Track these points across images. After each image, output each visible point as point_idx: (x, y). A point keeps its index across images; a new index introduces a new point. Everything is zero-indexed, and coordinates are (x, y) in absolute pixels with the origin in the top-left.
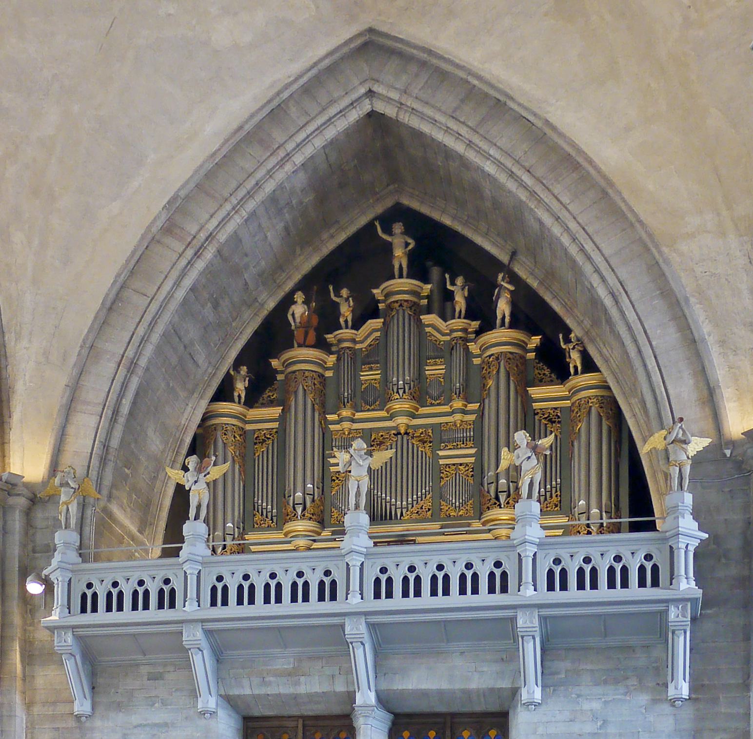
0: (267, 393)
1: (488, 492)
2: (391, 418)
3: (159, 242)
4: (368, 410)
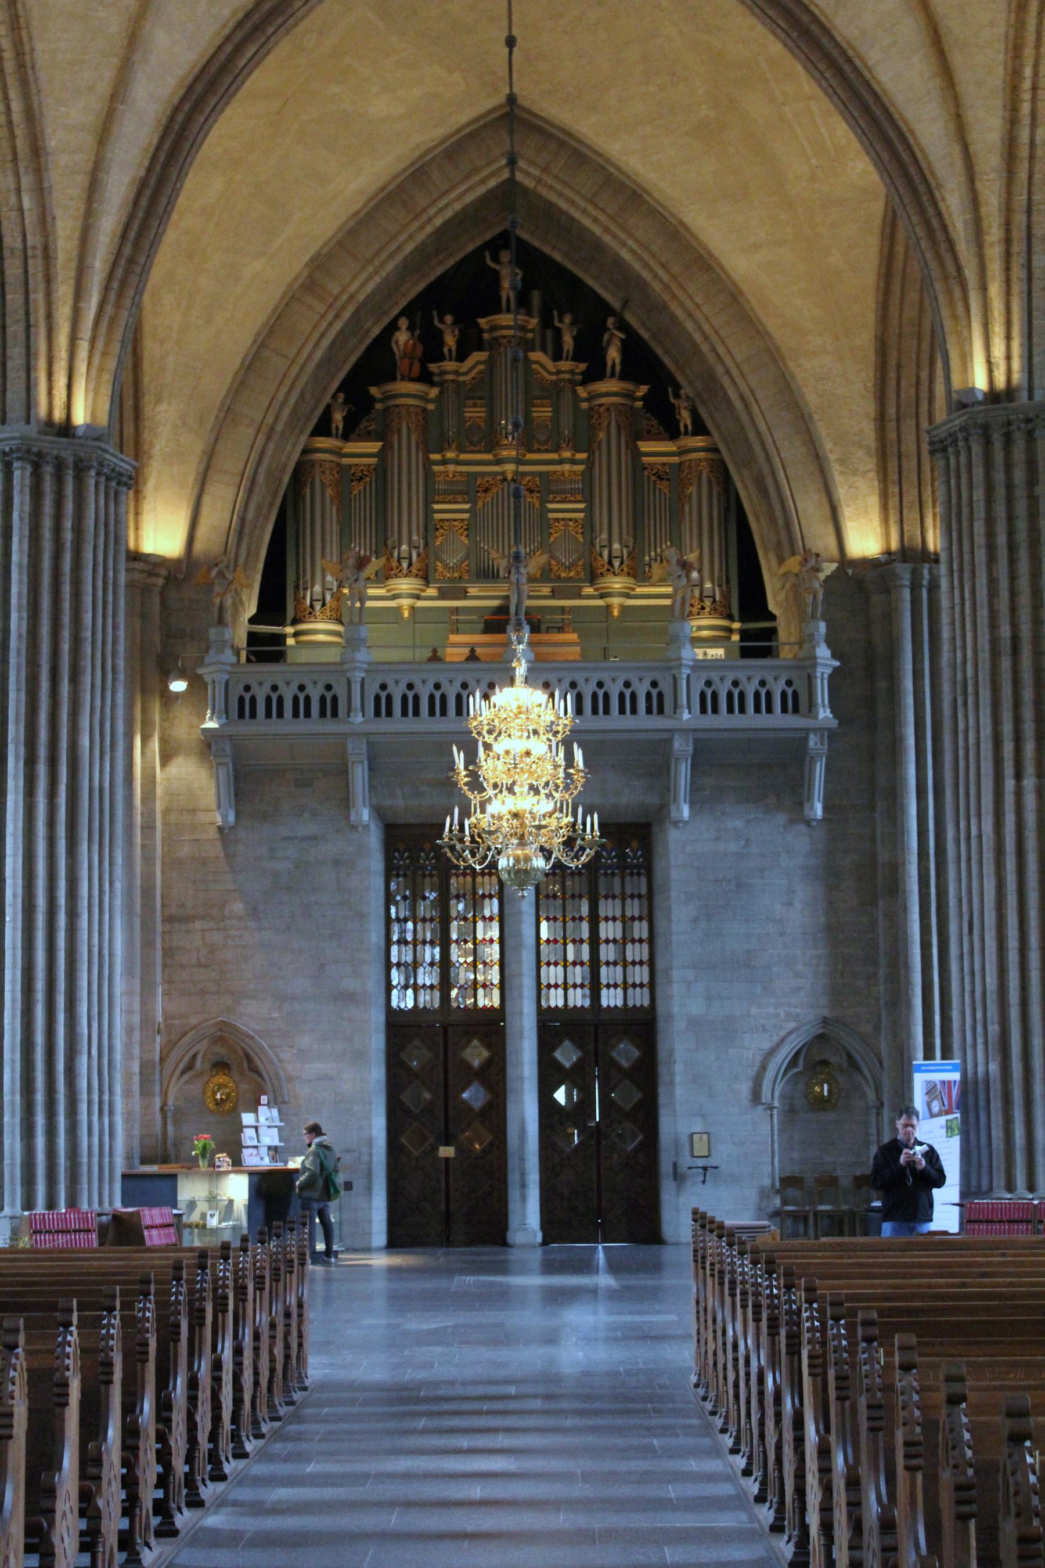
0: (364, 424)
1: (601, 555)
3: (298, 300)
4: (472, 452)
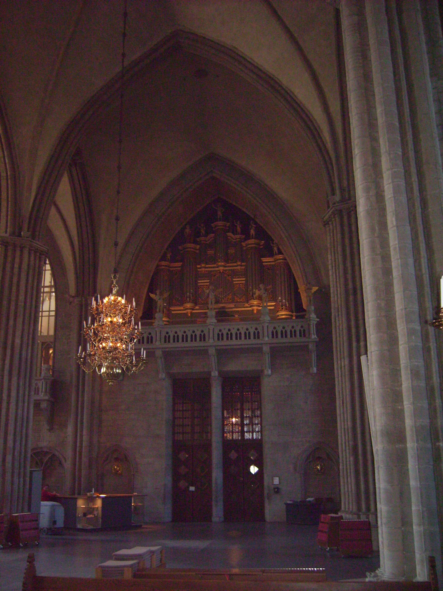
1: (250, 294)
2: (217, 267)
